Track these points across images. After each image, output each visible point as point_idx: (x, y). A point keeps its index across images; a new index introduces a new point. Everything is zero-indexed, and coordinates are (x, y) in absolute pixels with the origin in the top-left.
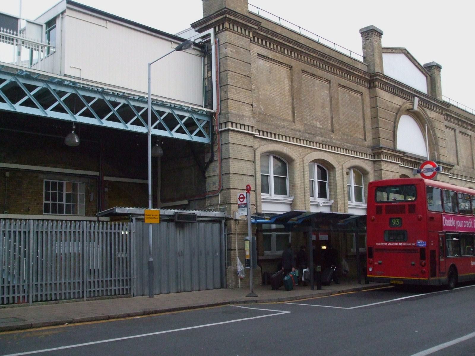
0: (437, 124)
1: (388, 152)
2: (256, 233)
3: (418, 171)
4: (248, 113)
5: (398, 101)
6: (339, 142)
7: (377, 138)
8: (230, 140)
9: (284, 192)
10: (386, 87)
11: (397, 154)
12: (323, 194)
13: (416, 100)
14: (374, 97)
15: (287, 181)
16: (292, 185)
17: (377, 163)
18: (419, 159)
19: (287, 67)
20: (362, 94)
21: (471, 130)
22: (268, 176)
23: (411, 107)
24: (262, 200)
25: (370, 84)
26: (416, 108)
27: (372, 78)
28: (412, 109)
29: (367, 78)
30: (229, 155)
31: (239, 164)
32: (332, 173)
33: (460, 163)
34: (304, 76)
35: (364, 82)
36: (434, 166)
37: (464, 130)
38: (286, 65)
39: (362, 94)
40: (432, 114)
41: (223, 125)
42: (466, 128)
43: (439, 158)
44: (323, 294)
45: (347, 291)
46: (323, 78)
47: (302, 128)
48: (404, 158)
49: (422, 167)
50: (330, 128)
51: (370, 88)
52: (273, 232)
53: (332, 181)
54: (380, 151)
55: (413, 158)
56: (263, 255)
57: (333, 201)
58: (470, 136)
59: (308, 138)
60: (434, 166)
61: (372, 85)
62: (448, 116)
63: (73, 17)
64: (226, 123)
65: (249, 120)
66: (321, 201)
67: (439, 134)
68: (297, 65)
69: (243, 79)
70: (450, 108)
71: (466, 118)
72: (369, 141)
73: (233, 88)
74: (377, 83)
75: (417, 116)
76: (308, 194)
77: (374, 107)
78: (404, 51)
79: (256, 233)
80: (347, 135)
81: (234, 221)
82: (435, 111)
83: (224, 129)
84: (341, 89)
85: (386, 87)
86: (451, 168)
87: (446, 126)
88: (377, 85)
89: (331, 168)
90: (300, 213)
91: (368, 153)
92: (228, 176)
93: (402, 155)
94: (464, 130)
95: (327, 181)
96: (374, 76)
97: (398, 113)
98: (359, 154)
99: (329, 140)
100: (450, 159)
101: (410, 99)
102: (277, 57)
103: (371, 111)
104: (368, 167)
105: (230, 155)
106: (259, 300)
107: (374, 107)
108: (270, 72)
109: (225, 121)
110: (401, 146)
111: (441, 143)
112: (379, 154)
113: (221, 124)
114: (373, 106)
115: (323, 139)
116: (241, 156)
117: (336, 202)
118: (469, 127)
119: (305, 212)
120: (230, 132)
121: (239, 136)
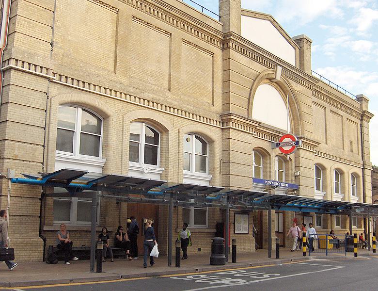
0: (302, 98)
1: (239, 119)
2: (40, 197)
3: (277, 145)
4: (43, 52)
5: (257, 67)
6: (176, 103)
7: (226, 104)
8: (11, 81)
9: (154, 162)
10: (268, 64)
11: (250, 123)
12: (203, 168)
13: (279, 69)
14: (226, 59)
15: (101, 140)
16: (105, 144)
17: (226, 131)
18: (279, 132)
19: (112, 10)
20: (213, 54)
21: (342, 110)
22: (73, 131)
23: (273, 76)
24: (56, 159)
25: (223, 45)
26: (278, 78)
27: (225, 39)
28: (274, 78)
29: (221, 37)
30: (8, 99)
31: (22, 111)
32: (164, 137)
33: (328, 141)
34: (135, 23)
35: (216, 41)
36: (293, 139)
37: (335, 109)
38: (111, 7)
39: (213, 54)
40: (297, 87)
41: (7, 62)
42: (337, 108)
43: (303, 133)
44: (147, 275)
45: (138, 276)
46: (137, 18)
47: (125, 81)
48: (259, 128)
49: (281, 140)
50: (167, 86)
51: (223, 49)
52: (191, 207)
53: (164, 145)
54: (229, 117)
55: (272, 130)
56: (52, 225)
57: (163, 169)
58: (342, 116)
59: (133, 93)
60: (293, 139)
61: (226, 46)
62: (317, 92)
63: (213, 77)
64: (9, 60)
65: (43, 60)
66: (201, 174)
67: (304, 109)
68: (178, 33)
69: (42, 12)
70: (320, 84)
71: (337, 97)
72: (218, 107)
73: (25, 21)
74: (231, 44)
75: (281, 88)
76: (126, 156)
77: (226, 70)
78: (270, 18)
79: (40, 197)
80: (189, 96)
81: (7, 180)
82: (302, 85)
83: (7, 66)
84: (184, 46)
85: (268, 64)
86: (317, 145)
87: (315, 103)
88: (231, 46)
89: (324, 169)
90: (347, 203)
91: (215, 119)
92: (4, 124)
93: (257, 125)
94: (335, 109)
95: (159, 146)
96: (228, 36)
97: (256, 80)
98: (166, 108)
99: (162, 98)
100: (318, 136)
101: (272, 68)
102: (145, 17)
103: (223, 74)
104: (214, 133)
105: (9, 98)
106: (12, 284)
107: (226, 70)
108: (87, 12)
109: (8, 58)
110: (256, 115)
111: (306, 118)
112: (228, 121)
113: (5, 61)
114: (225, 69)
115: (154, 96)
116: (26, 102)
117: (167, 170)
118: (340, 107)
119: (165, 182)
120: (13, 71)
121: (27, 78)
